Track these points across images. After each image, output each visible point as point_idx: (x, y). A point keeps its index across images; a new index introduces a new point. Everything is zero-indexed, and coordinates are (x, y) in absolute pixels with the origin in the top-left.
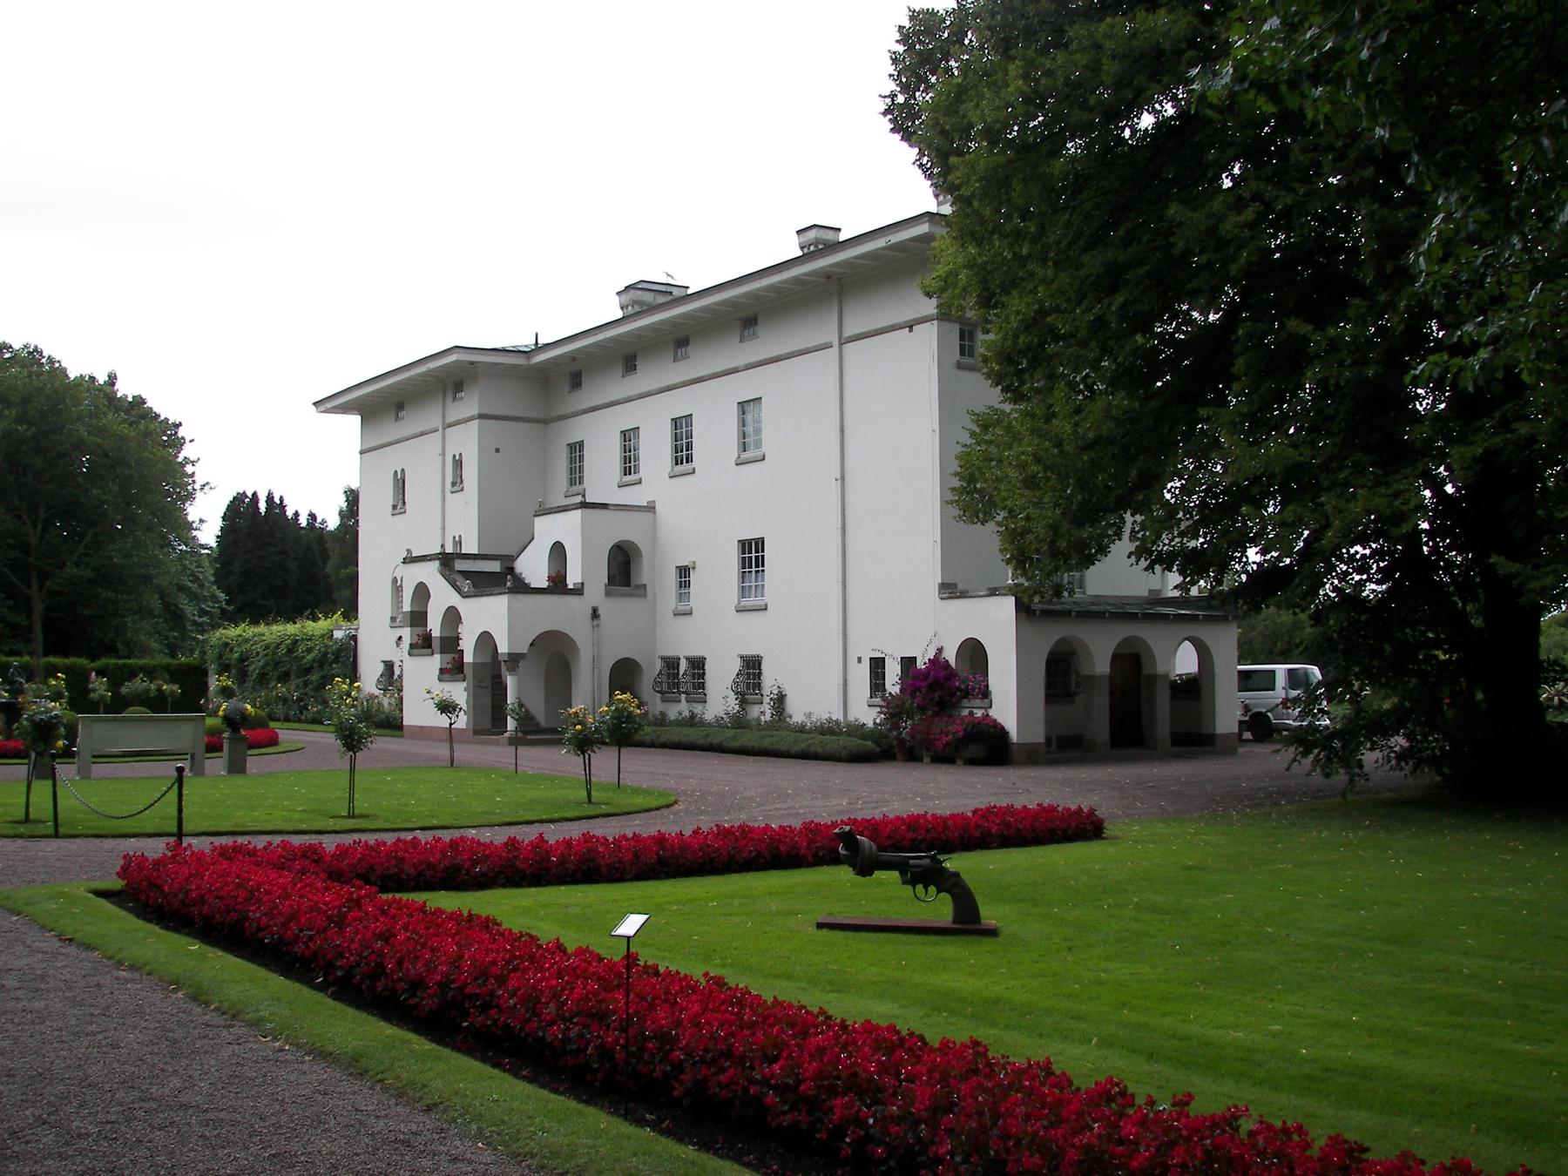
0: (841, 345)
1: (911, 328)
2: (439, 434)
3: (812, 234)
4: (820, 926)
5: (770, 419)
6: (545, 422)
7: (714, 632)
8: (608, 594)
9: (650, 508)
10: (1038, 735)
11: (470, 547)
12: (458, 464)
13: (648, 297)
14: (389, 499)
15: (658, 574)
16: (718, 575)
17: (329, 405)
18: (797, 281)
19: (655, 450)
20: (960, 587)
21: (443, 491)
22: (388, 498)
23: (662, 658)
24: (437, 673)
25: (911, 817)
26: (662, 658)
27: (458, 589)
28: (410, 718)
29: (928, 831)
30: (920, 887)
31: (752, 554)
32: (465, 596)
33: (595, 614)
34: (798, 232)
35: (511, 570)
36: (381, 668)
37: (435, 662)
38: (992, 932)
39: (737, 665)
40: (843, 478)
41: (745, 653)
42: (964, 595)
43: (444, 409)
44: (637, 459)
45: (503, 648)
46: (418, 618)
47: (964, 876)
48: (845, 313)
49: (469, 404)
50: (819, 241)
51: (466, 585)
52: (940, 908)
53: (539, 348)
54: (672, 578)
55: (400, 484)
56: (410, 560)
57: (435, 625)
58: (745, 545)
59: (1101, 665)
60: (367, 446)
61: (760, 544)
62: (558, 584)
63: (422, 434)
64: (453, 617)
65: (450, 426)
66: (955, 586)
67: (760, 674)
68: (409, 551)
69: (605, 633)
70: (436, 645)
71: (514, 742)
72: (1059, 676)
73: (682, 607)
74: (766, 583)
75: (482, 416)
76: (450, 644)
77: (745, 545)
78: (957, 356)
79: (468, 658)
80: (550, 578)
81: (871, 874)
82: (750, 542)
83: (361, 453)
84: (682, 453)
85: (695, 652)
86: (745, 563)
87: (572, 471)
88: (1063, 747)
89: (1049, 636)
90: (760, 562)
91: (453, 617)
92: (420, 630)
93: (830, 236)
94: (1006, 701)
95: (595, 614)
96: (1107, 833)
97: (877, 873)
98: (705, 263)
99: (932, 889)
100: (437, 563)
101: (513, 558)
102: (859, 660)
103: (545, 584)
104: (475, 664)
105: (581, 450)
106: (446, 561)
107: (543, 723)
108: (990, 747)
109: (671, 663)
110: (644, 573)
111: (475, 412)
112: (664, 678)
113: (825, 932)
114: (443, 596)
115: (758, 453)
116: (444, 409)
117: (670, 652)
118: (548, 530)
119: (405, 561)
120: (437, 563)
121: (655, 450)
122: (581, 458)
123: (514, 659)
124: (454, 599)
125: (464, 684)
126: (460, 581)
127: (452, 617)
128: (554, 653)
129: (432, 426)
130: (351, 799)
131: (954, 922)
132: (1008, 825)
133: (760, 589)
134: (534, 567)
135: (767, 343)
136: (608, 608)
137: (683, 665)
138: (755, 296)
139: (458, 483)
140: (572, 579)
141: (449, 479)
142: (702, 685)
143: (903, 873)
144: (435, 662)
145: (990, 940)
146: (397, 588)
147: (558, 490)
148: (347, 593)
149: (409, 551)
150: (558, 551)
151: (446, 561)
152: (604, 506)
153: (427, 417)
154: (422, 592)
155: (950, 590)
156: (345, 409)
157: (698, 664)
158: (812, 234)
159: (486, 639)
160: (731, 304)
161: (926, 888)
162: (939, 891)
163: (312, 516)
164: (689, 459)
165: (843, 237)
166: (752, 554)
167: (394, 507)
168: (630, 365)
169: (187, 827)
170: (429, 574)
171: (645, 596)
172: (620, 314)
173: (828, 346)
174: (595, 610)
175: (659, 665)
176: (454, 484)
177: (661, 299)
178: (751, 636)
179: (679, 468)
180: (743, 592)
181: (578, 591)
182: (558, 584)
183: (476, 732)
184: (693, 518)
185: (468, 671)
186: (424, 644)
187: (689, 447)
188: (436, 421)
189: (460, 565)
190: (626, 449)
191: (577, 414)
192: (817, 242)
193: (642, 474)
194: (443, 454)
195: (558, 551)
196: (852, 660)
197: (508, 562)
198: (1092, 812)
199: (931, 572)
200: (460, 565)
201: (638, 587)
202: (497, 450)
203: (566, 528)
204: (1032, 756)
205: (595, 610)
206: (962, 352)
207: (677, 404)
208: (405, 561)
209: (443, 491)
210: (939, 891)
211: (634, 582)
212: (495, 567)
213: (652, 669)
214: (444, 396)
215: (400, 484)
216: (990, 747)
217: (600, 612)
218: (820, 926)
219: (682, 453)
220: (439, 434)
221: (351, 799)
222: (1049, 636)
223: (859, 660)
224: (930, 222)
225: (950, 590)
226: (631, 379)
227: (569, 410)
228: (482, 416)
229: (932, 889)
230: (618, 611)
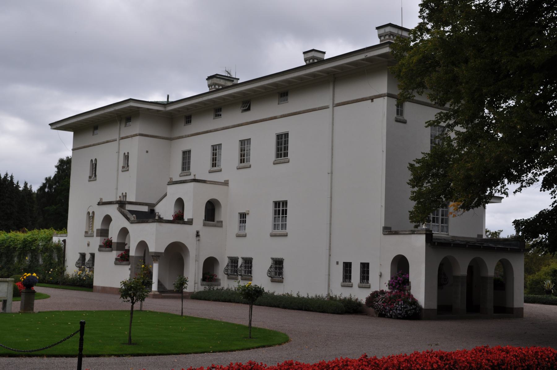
2: (328, 112)
3: (388, 29)
6: (171, 139)
7: (259, 247)
8: (204, 225)
9: (226, 183)
11: (131, 198)
12: (127, 157)
13: (222, 82)
15: (228, 215)
17: (59, 125)
18: (300, 78)
19: (230, 155)
20: (393, 229)
21: (118, 170)
22: (87, 171)
27: (128, 219)
31: (281, 209)
33: (198, 235)
36: (78, 256)
37: (114, 254)
39: (269, 263)
40: (332, 173)
42: (396, 233)
43: (120, 130)
44: (249, 155)
45: (152, 249)
46: (104, 233)
48: (336, 90)
49: (136, 127)
50: (314, 58)
51: (132, 217)
54: (237, 218)
55: (94, 166)
56: (101, 203)
58: (277, 204)
59: (463, 271)
61: (285, 203)
62: (179, 218)
63: (107, 142)
64: (124, 232)
65: (122, 138)
66: (390, 228)
67: (251, 267)
68: (101, 199)
69: (203, 244)
70: (114, 246)
71: (155, 296)
72: (442, 276)
73: (242, 232)
74: (287, 223)
76: (122, 246)
77: (277, 204)
78: (396, 115)
79: (132, 253)
83: (73, 150)
84: (244, 157)
87: (184, 164)
88: (443, 311)
90: (285, 212)
91: (124, 232)
93: (319, 55)
94: (419, 289)
95: (198, 235)
100: (117, 206)
101: (154, 205)
102: (337, 263)
103: (172, 218)
106: (122, 204)
108: (413, 313)
109: (233, 261)
111: (384, 90)
112: (230, 268)
114: (119, 222)
116: (120, 130)
119: (99, 204)
120: (117, 206)
121: (230, 155)
123: (157, 256)
125: (129, 267)
126: (129, 215)
128: (176, 254)
129: (113, 138)
133: (284, 226)
134: (166, 210)
135: (295, 103)
137: (240, 262)
138: (288, 81)
139: (126, 167)
144: (114, 254)
146: (91, 217)
147: (176, 172)
149: (101, 199)
150: (180, 202)
151: (122, 204)
153: (112, 133)
155: (388, 231)
157: (248, 262)
158: (310, 55)
159: (143, 245)
160: (275, 84)
163: (26, 184)
164: (286, 155)
165: (326, 57)
166: (281, 209)
167: (90, 177)
169: (84, 353)
170: (113, 211)
171: (221, 226)
173: (327, 107)
174: (198, 232)
176: (123, 167)
177: (229, 84)
178: (278, 248)
179: (243, 165)
180: (275, 227)
181: (190, 222)
184: (248, 190)
186: (107, 245)
187: (286, 148)
188: (116, 137)
190: (214, 154)
192: (313, 58)
193: (251, 162)
194: (119, 152)
195: (180, 202)
196: (333, 263)
200: (129, 207)
202: (147, 152)
203: (186, 192)
204: (196, 297)
205: (198, 232)
206: (398, 114)
207: (244, 133)
208: (99, 204)
209: (118, 170)
211: (217, 219)
212: (145, 209)
213: (224, 263)
214: (120, 124)
215: (94, 166)
216: (413, 313)
217: (200, 234)
219: (244, 157)
223: (337, 263)
224: (390, 47)
225: (388, 231)
226: (247, 113)
230: (208, 233)
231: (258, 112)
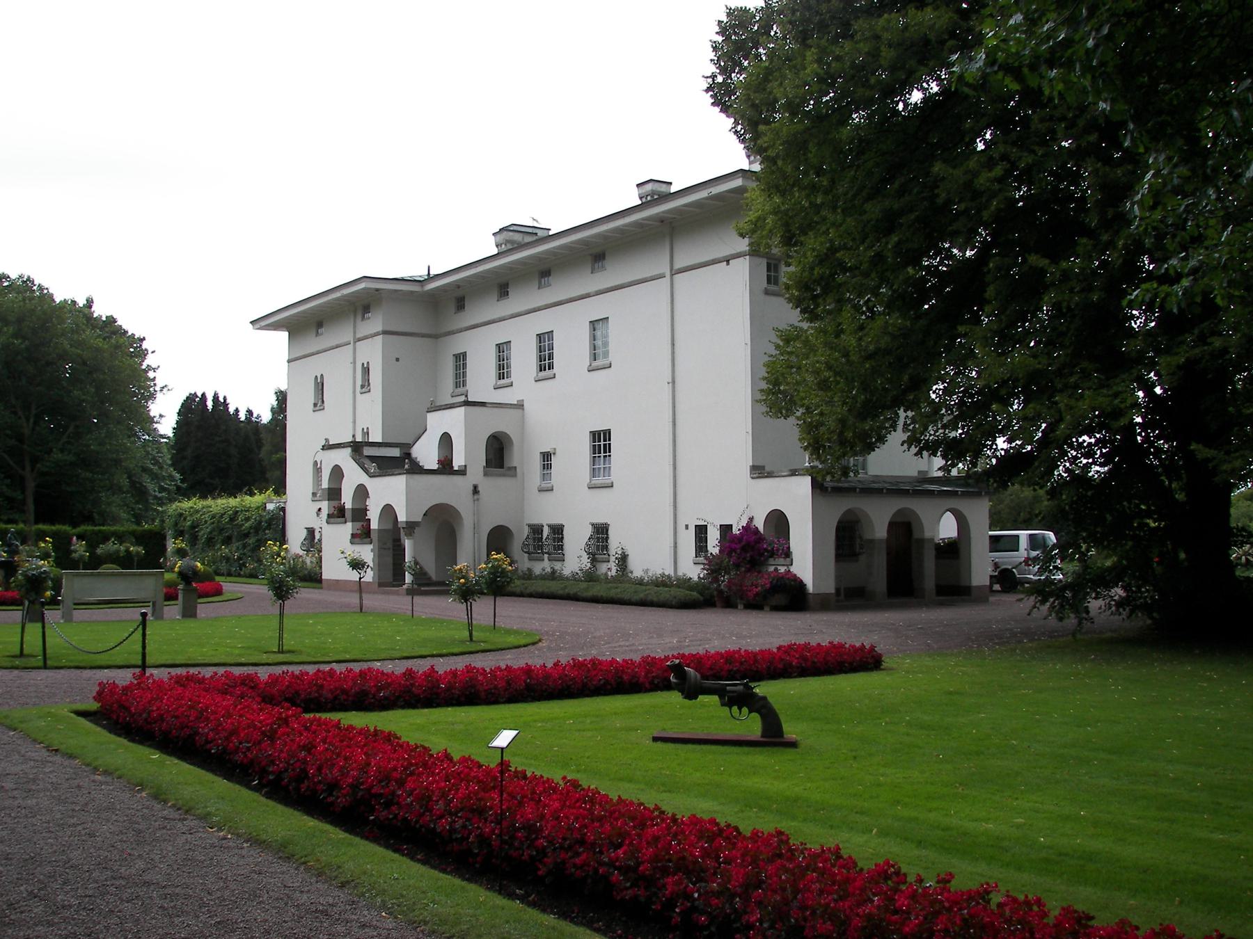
0: (672, 275)
1: (728, 262)
2: (351, 346)
3: (649, 187)
4: (655, 739)
5: (615, 335)
6: (436, 337)
7: (571, 505)
8: (486, 474)
9: (520, 406)
10: (829, 587)
11: (376, 437)
12: (366, 370)
13: (518, 237)
14: (311, 399)
15: (526, 459)
16: (574, 459)
17: (263, 323)
18: (637, 224)
19: (524, 359)
20: (767, 469)
21: (354, 392)
22: (310, 397)
23: (529, 526)
24: (349, 537)
25: (728, 652)
26: (529, 526)
27: (366, 471)
28: (328, 573)
29: (741, 663)
30: (735, 709)
31: (601, 442)
32: (371, 476)
33: (475, 490)
34: (638, 185)
35: (408, 455)
36: (304, 533)
37: (347, 529)
38: (793, 745)
39: (589, 531)
40: (674, 382)
41: (595, 521)
42: (770, 475)
43: (355, 327)
44: (509, 366)
45: (402, 518)
46: (334, 493)
47: (770, 700)
48: (676, 250)
49: (375, 323)
50: (654, 193)
51: (373, 467)
52: (751, 725)
53: (431, 278)
54: (537, 462)
55: (320, 386)
56: (328, 447)
57: (347, 499)
58: (595, 435)
59: (880, 531)
60: (293, 356)
61: (607, 434)
62: (446, 467)
63: (337, 347)
64: (362, 492)
65: (359, 340)
66: (763, 468)
67: (607, 538)
68: (327, 440)
69: (484, 505)
70: (348, 515)
71: (411, 592)
72: (846, 540)
73: (545, 485)
74: (612, 465)
75: (385, 333)
76: (360, 514)
77: (595, 435)
78: (765, 284)
79: (374, 525)
80: (439, 462)
81: (696, 698)
82: (599, 432)
83: (289, 361)
84: (545, 362)
85: (556, 521)
86: (595, 450)
87: (457, 376)
88: (850, 596)
89: (839, 508)
90: (607, 448)
91: (362, 492)
92: (335, 503)
93: (663, 188)
94: (804, 560)
95: (475, 490)
96: (884, 665)
97: (701, 697)
98: (564, 210)
99: (745, 710)
100: (349, 450)
101: (410, 446)
102: (687, 527)
103: (435, 467)
104: (379, 530)
105: (464, 359)
106: (357, 448)
107: (434, 577)
108: (791, 597)
109: (536, 530)
110: (515, 458)
111: (380, 329)
112: (531, 542)
113: (659, 744)
114: (354, 476)
115: (606, 362)
116: (355, 327)
117: (536, 521)
118: (438, 423)
119: (324, 448)
120: (349, 450)
121: (524, 359)
122: (465, 365)
123: (411, 527)
124: (363, 478)
125: (371, 546)
126: (368, 464)
127: (362, 493)
128: (442, 522)
129: (345, 340)
130: (281, 638)
131: (762, 736)
132: (805, 659)
133: (607, 471)
134: (426, 453)
135: (613, 274)
136: (486, 485)
137: (546, 531)
138: (604, 236)
139: (366, 385)
140: (457, 463)
141: (359, 383)
142: (561, 547)
143: (721, 697)
144: (347, 529)
145: (791, 751)
146: (317, 469)
147: (446, 391)
148: (277, 473)
149: (327, 440)
150: (446, 440)
151: (357, 448)
152: (483, 404)
153: (342, 333)
154: (337, 473)
155: (759, 471)
156: (276, 326)
157: (558, 531)
158: (649, 187)
159: (388, 511)
160: (584, 242)
161: (740, 709)
162: (750, 712)
163: (250, 412)
164: (551, 367)
165: (673, 189)
166: (601, 442)
167: (315, 405)
168: (503, 291)
169: (149, 660)
170: (343, 458)
171: (515, 476)
172: (495, 251)
173: (662, 276)
174: (475, 487)
175: (526, 531)
176: (362, 387)
177: (528, 239)
178: (600, 508)
179: (543, 374)
180: (594, 472)
181: (462, 472)
182: (446, 467)
183: (381, 585)
184: (554, 414)
185: (374, 536)
186: (338, 514)
187: (551, 357)
188: (348, 336)
189: (368, 451)
190: (500, 359)
191: (461, 331)
192: (653, 193)
193: (513, 379)
194: (354, 362)
195: (446, 440)
196: (681, 527)
197: (406, 449)
198: (872, 648)
199: (744, 457)
200: (368, 451)
201: (510, 468)
202: (397, 360)
203: (452, 421)
204: (825, 604)
205: (475, 487)
206: (769, 281)
207: (541, 322)
208: (324, 448)
209: (354, 392)
210: (750, 712)
211: (506, 464)
212: (396, 452)
213: (521, 534)
214: (355, 317)
215: (320, 386)
216: (791, 597)
217: (480, 489)
218: (655, 739)
219: (545, 362)
220: (351, 346)
221: (281, 638)
222: (839, 508)
223: (687, 527)
224: (743, 177)
225: (759, 471)
226: (504, 302)
227: (455, 328)
228: (385, 333)
229: (745, 710)
230: (494, 488)
231: (518, 300)
